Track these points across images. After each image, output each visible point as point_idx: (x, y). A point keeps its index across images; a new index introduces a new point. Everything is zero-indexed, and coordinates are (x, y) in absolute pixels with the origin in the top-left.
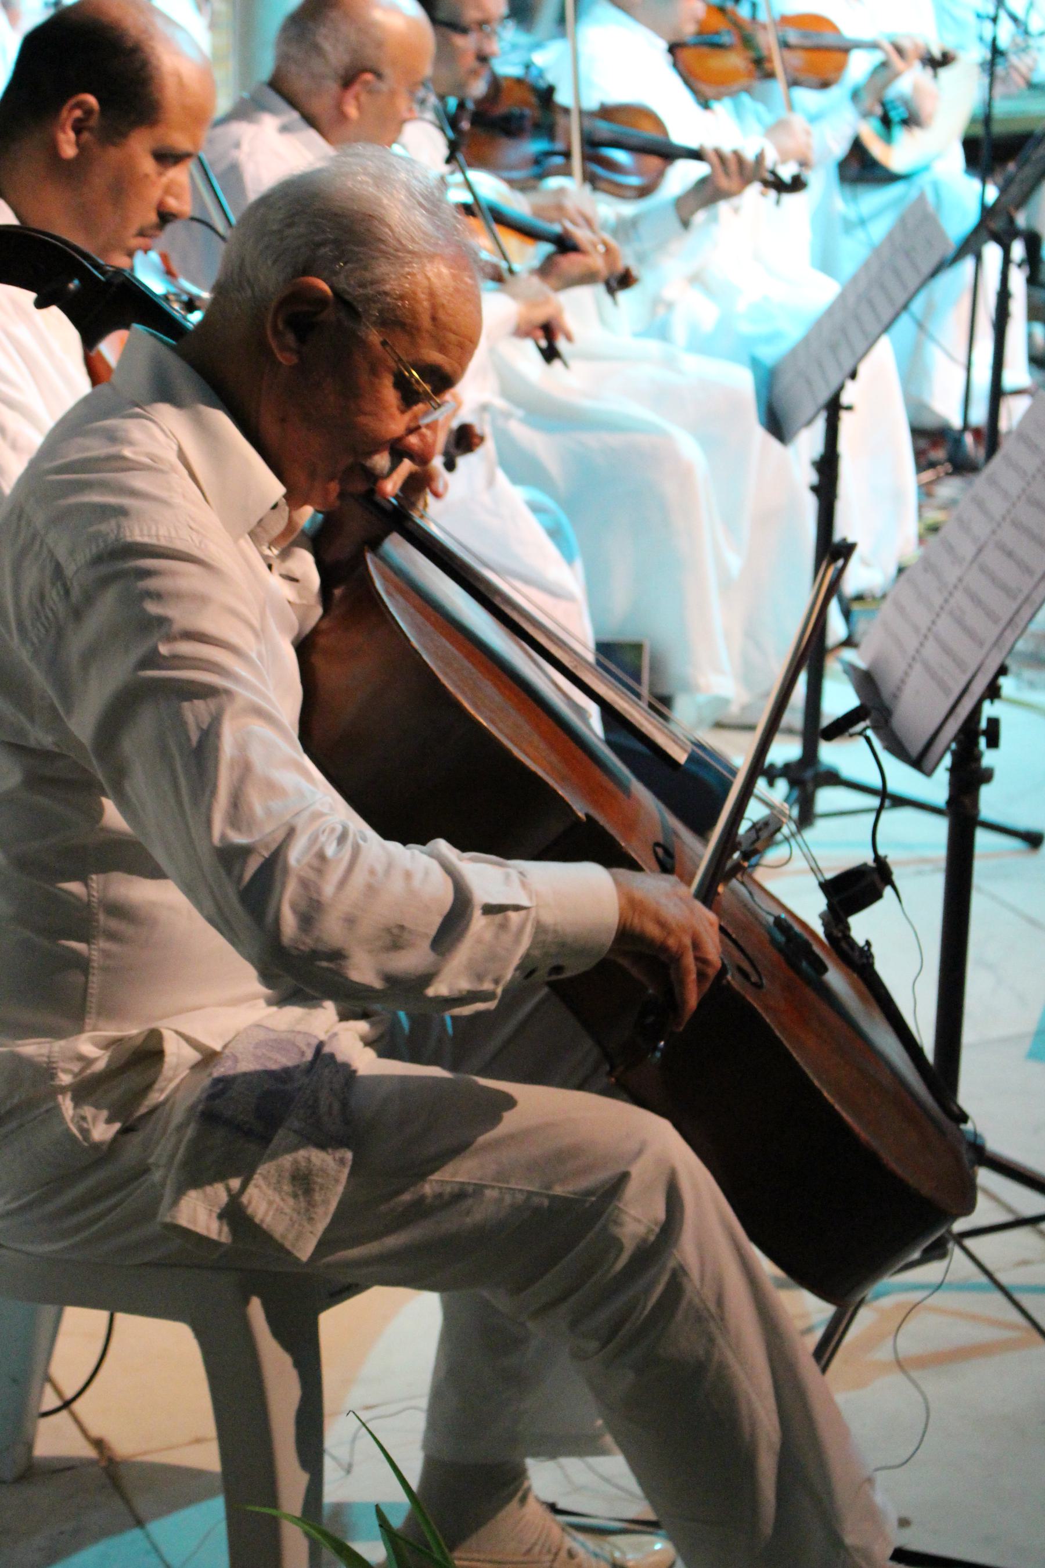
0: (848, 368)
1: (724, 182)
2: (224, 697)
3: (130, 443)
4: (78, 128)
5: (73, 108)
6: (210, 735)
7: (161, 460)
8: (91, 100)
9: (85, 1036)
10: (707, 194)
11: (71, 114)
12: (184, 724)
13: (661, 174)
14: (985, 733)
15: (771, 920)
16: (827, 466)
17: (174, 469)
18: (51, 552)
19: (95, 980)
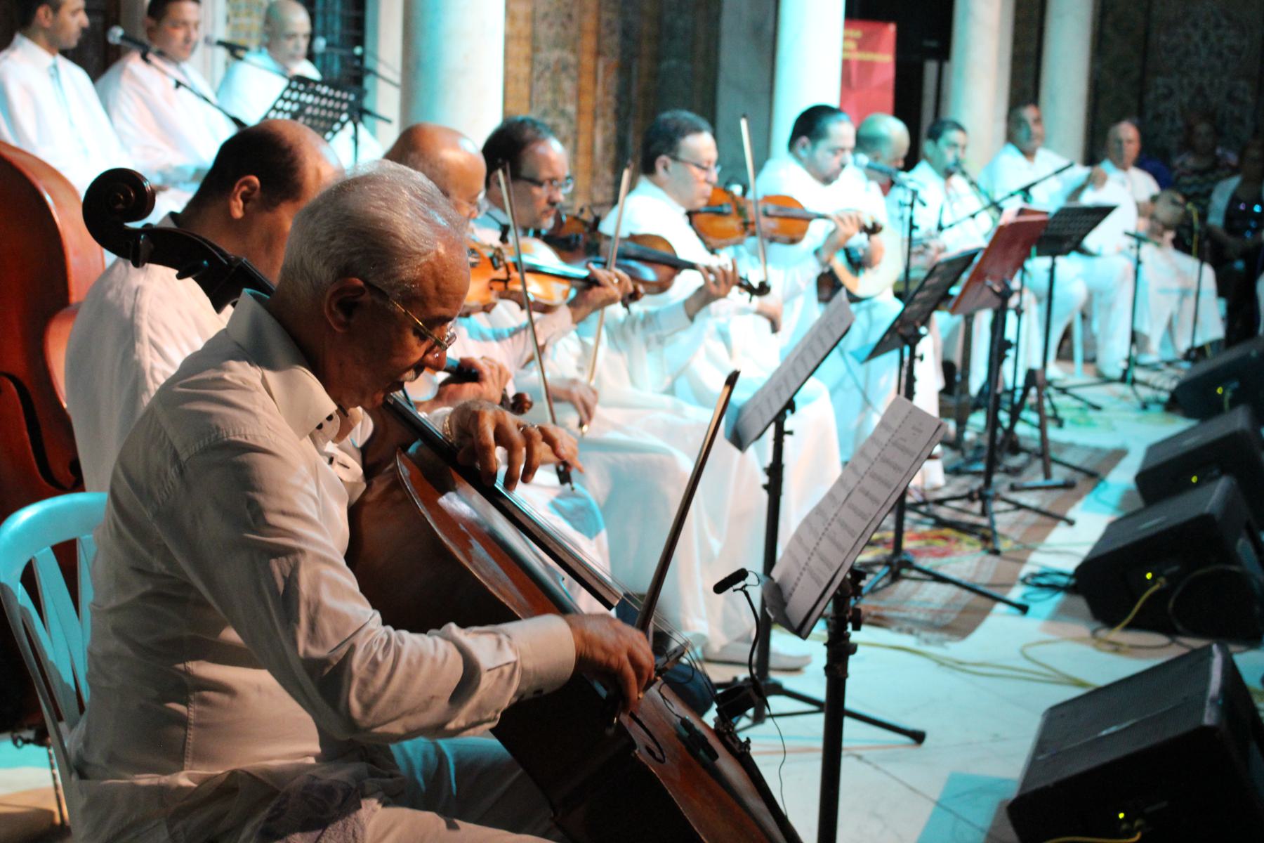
0: (785, 399)
1: (714, 289)
2: (300, 555)
3: (230, 370)
4: (245, 198)
5: (241, 185)
6: (292, 581)
7: (250, 383)
8: (256, 180)
9: (183, 773)
10: (704, 298)
11: (240, 190)
12: (272, 574)
13: (671, 279)
14: (851, 620)
15: (679, 720)
16: (775, 471)
17: (259, 390)
18: (171, 443)
19: (192, 734)
